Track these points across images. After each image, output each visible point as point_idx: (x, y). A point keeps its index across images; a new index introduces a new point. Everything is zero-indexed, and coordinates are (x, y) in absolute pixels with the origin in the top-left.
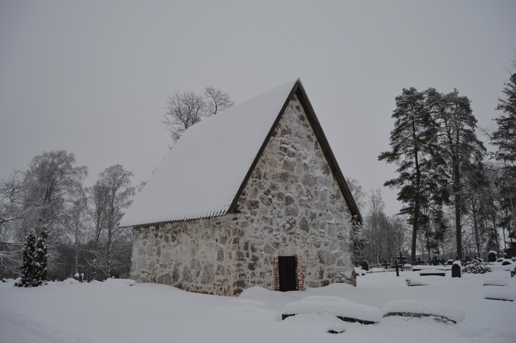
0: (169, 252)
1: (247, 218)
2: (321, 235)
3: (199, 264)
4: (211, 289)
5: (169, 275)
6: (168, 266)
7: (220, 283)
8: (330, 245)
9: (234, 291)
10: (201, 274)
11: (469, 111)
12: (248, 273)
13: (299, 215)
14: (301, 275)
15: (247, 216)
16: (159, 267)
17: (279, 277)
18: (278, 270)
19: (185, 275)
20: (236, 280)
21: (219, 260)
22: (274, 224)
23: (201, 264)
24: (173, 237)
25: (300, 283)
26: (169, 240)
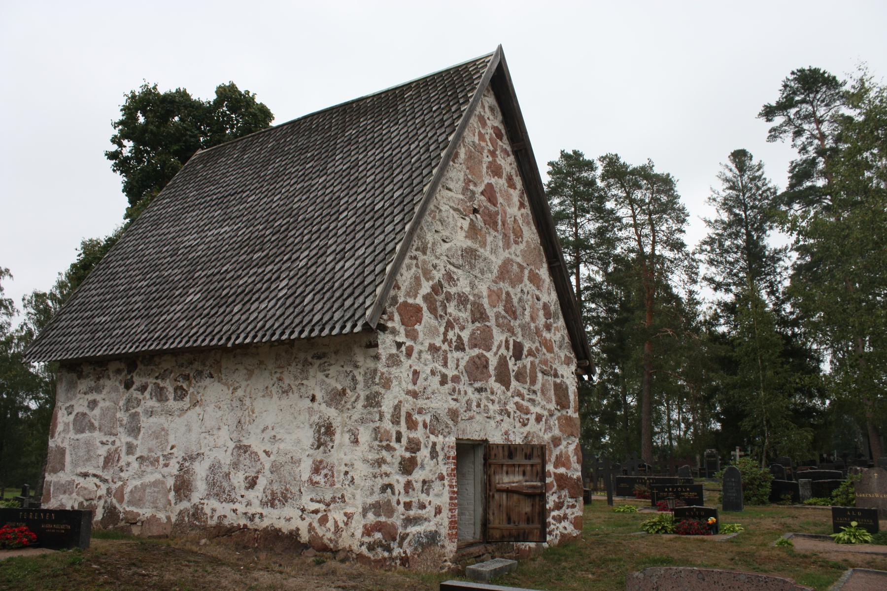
0: (166, 426)
1: (399, 345)
6: (162, 462)
8: (544, 420)
9: (365, 526)
10: (262, 482)
11: (673, 198)
12: (398, 481)
13: (494, 349)
15: (400, 339)
16: (135, 465)
18: (454, 476)
20: (371, 500)
21: (318, 447)
26: (166, 397)
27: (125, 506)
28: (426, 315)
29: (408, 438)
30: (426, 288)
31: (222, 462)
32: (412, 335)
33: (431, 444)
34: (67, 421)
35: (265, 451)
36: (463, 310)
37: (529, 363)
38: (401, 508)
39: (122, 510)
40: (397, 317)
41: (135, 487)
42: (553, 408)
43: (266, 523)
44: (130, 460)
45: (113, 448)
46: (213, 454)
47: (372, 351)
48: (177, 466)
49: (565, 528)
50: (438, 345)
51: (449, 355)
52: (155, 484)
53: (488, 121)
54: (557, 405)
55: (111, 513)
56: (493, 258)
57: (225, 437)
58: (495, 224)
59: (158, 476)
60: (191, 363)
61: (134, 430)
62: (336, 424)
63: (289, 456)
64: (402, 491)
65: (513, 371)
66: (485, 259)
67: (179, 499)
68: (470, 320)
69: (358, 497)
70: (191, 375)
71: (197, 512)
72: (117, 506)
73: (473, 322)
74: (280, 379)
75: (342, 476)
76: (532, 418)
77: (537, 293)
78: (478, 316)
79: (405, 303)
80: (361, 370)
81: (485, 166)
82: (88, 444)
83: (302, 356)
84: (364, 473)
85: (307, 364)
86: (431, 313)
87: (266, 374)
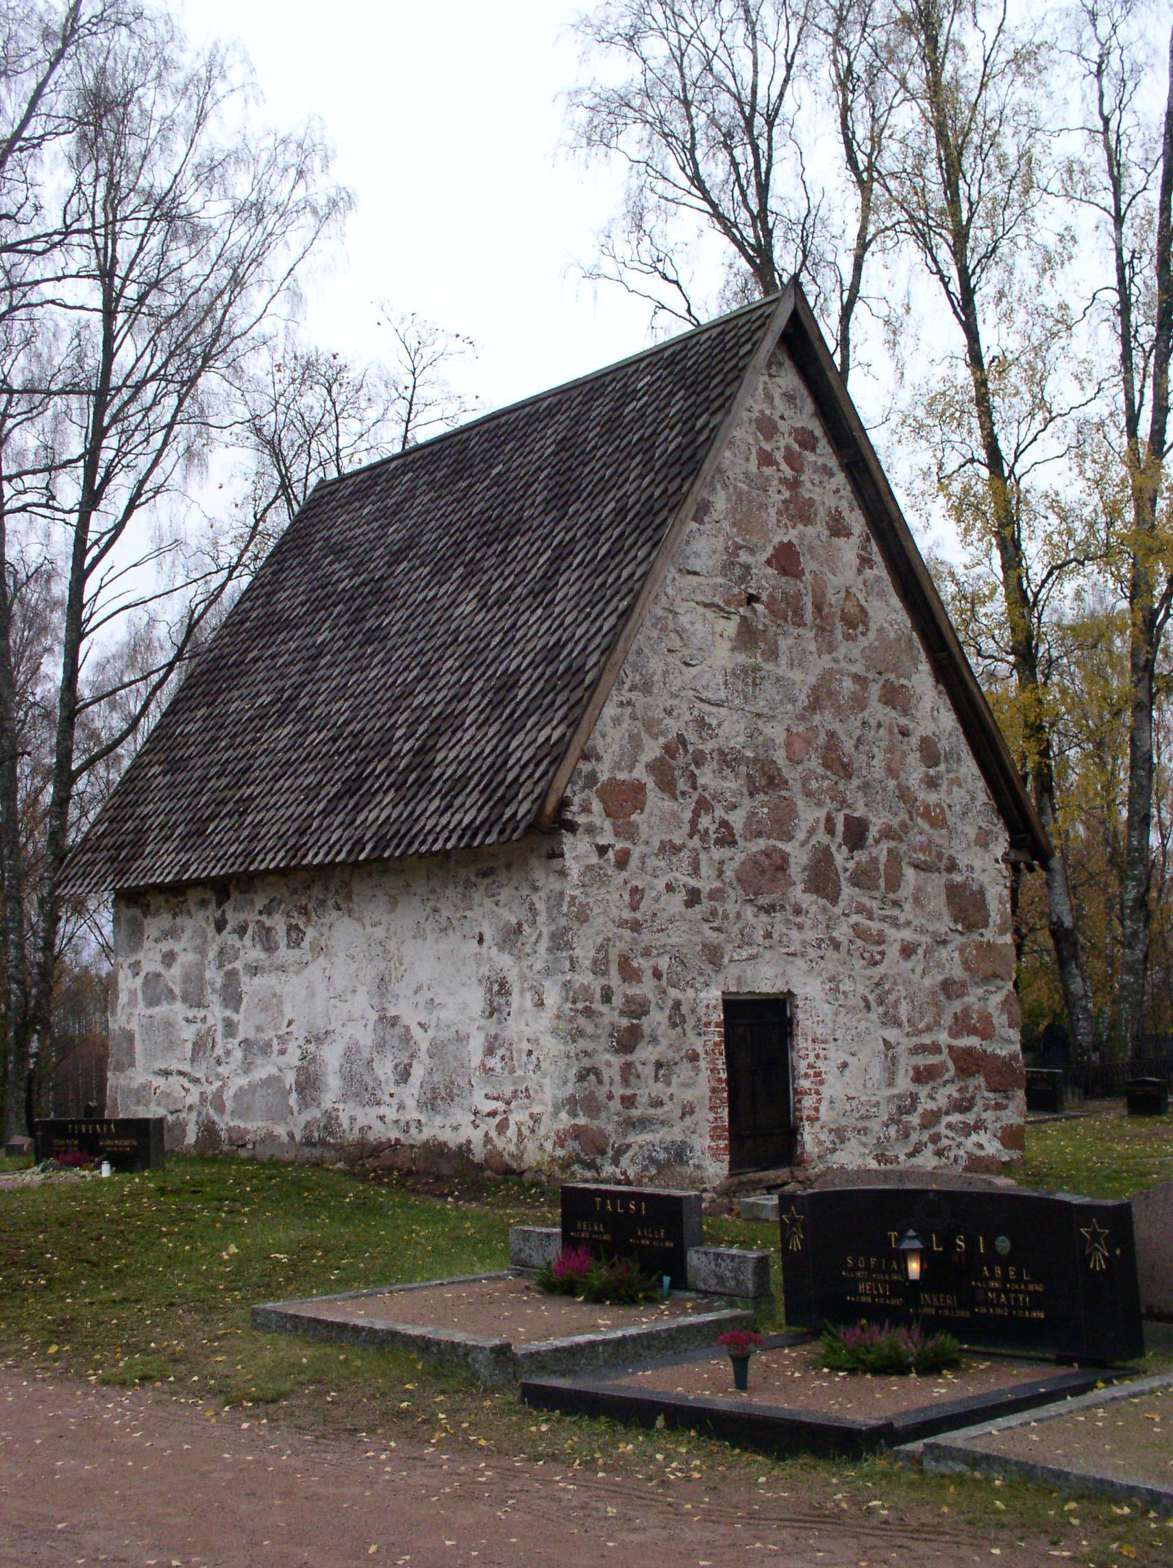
0: (278, 989)
1: (602, 850)
2: (887, 913)
3: (406, 1038)
4: (462, 1129)
5: (278, 1080)
6: (276, 1047)
7: (500, 1106)
8: (920, 951)
10: (418, 1072)
12: (609, 1064)
13: (801, 835)
14: (811, 1072)
17: (728, 1081)
19: (349, 1078)
21: (491, 1014)
22: (703, 872)
23: (416, 1032)
24: (291, 928)
25: (808, 1102)
27: (227, 1118)
28: (653, 795)
29: (626, 996)
30: (652, 750)
31: (361, 1042)
32: (628, 831)
33: (670, 1003)
34: (133, 987)
35: (420, 1024)
36: (731, 776)
37: (885, 852)
38: (616, 1105)
39: (223, 1126)
40: (597, 806)
41: (241, 1088)
42: (943, 929)
43: (426, 1134)
44: (230, 1046)
45: (204, 1027)
46: (350, 1030)
47: (556, 863)
48: (298, 1052)
49: (981, 1146)
50: (678, 842)
51: (703, 857)
52: (269, 1082)
53: (781, 423)
54: (956, 921)
55: (209, 1131)
56: (796, 675)
57: (361, 1003)
58: (798, 611)
59: (271, 1070)
60: (308, 887)
61: (232, 997)
62: (512, 977)
63: (453, 1029)
64: (617, 1078)
65: (846, 870)
66: (778, 680)
67: (304, 1104)
68: (745, 792)
69: (547, 1089)
70: (310, 906)
71: (330, 1122)
72: (216, 1118)
73: (751, 795)
74: (436, 910)
75: (525, 1057)
76: (893, 951)
77: (903, 721)
78: (764, 782)
79: (612, 781)
80: (543, 894)
81: (773, 511)
82: (169, 1025)
83: (463, 874)
84: (554, 1052)
85: (469, 885)
86: (662, 790)
87: (416, 901)
